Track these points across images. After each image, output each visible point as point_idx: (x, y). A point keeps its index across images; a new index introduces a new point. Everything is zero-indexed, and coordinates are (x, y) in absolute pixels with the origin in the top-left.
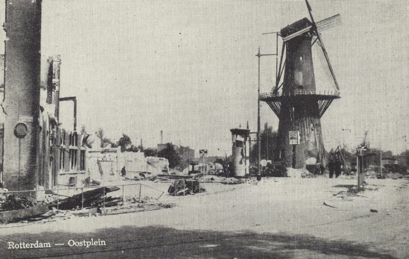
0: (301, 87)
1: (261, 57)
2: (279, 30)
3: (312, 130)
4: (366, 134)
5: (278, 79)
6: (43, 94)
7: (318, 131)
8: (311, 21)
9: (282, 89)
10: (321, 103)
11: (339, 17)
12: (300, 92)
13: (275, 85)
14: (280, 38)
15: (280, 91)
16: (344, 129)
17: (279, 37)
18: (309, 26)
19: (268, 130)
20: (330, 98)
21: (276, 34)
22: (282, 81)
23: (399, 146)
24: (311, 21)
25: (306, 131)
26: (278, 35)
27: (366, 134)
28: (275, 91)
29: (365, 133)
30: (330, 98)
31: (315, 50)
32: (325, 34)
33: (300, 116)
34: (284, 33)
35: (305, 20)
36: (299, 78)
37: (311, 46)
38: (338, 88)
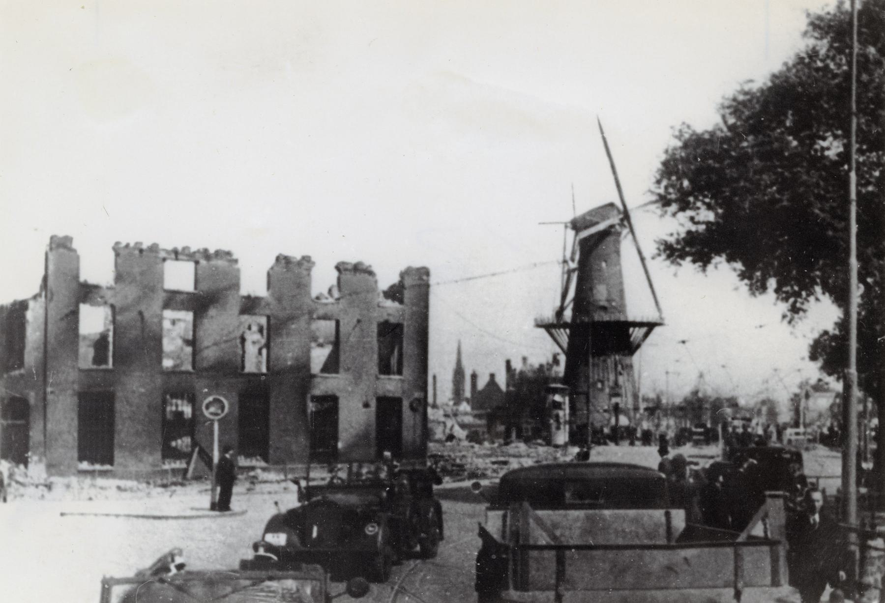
0: (604, 309)
5: (564, 296)
6: (265, 327)
7: (628, 374)
10: (637, 333)
12: (606, 318)
14: (571, 233)
15: (568, 314)
16: (670, 370)
19: (742, 271)
20: (650, 326)
21: (562, 226)
22: (571, 294)
26: (566, 227)
28: (560, 313)
30: (650, 326)
31: (626, 246)
33: (602, 351)
34: (577, 225)
35: (612, 205)
36: (601, 293)
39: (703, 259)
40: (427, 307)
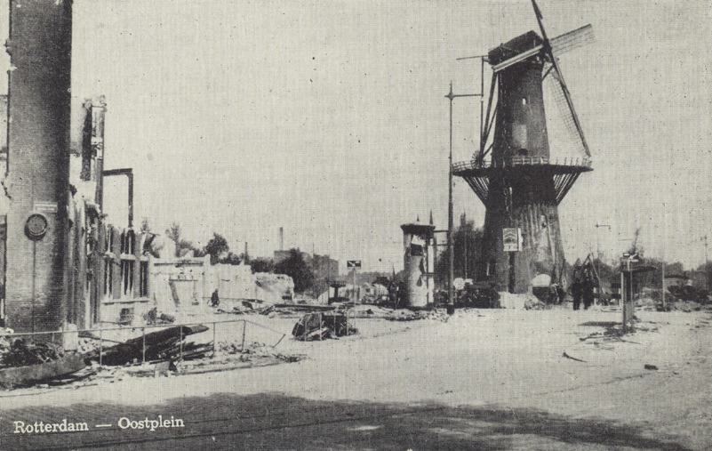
0: (524, 152)
1: (455, 100)
2: (486, 53)
3: (544, 226)
4: (637, 233)
5: (484, 138)
6: (76, 163)
7: (553, 227)
8: (541, 36)
9: (491, 154)
10: (559, 180)
11: (590, 30)
12: (523, 160)
13: (478, 148)
14: (488, 66)
15: (488, 158)
16: (599, 224)
17: (486, 64)
18: (537, 45)
20: (574, 172)
21: (480, 59)
22: (490, 140)
23: (694, 254)
24: (541, 36)
25: (533, 228)
26: (483, 60)
27: (637, 233)
28: (479, 158)
29: (635, 232)
30: (574, 172)
32: (566, 58)
33: (521, 202)
34: (495, 57)
35: (531, 34)
36: (521, 135)
37: (541, 80)
38: (588, 153)
39: (213, 294)
40: (68, 48)
